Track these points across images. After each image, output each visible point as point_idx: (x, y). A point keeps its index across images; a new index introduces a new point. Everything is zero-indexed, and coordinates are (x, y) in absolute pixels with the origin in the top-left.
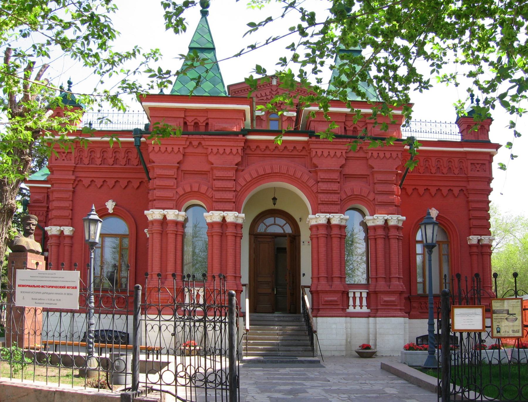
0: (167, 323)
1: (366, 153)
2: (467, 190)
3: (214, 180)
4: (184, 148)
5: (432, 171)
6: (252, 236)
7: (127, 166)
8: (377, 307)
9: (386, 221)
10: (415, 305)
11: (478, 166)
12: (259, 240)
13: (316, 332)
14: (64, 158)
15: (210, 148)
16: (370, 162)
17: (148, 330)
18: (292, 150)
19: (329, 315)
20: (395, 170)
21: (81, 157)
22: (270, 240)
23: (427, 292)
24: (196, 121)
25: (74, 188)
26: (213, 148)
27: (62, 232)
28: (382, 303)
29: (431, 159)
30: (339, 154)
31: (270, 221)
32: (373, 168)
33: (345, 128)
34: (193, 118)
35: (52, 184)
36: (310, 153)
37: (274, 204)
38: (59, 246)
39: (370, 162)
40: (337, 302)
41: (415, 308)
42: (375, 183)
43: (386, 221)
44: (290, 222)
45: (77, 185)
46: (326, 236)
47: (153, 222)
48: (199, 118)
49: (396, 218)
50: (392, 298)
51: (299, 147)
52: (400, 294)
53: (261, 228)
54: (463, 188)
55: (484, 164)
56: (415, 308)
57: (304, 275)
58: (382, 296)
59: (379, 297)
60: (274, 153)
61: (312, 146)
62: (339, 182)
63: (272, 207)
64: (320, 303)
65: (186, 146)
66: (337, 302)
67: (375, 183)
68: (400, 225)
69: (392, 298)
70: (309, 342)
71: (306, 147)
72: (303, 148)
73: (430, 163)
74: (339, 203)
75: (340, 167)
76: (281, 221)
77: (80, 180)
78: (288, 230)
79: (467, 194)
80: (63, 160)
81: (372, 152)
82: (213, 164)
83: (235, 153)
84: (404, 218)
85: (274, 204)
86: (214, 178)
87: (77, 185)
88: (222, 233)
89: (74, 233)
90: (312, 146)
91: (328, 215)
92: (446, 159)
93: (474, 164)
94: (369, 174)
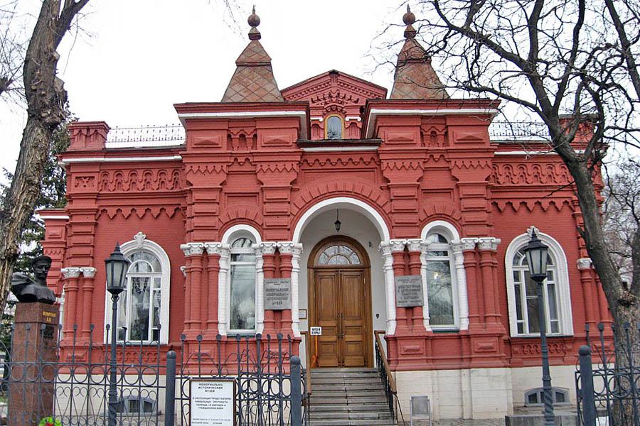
0: (97, 387)
1: (448, 162)
2: (572, 201)
3: (265, 203)
4: (424, 162)
5: (542, 180)
6: (312, 270)
7: (175, 190)
8: (398, 357)
9: (477, 245)
10: (516, 349)
11: (85, 180)
12: (320, 274)
13: (395, 393)
14: (85, 184)
15: (259, 165)
16: (260, 176)
17: (92, 396)
18: (439, 159)
19: (534, 364)
20: (289, 185)
21: (106, 181)
22: (334, 274)
23: (110, 342)
24: (242, 132)
25: (96, 220)
26: (262, 164)
27: (81, 274)
28: (476, 351)
29: (554, 166)
30: (415, 164)
31: (331, 250)
32: (458, 180)
33: (421, 133)
34: (238, 130)
35: (71, 216)
36: (380, 165)
37: (338, 229)
38: (77, 291)
39: (260, 176)
40: (492, 348)
41: (517, 353)
42: (461, 199)
43: (477, 245)
44: (357, 251)
45: (100, 215)
46: (200, 270)
47: (191, 258)
48: (246, 130)
49: (488, 241)
50: (79, 354)
51: (367, 159)
52: (426, 339)
53: (322, 260)
54: (568, 200)
55: (93, 177)
56: (517, 353)
57: (378, 315)
58: (402, 343)
59: (472, 342)
60: (347, 167)
61: (381, 157)
62: (218, 203)
63: (335, 233)
64: (399, 353)
65: (230, 164)
66: (492, 348)
67: (461, 199)
68: (494, 248)
69: (79, 354)
70: (387, 406)
71: (375, 158)
72: (372, 158)
73: (511, 171)
74: (418, 224)
75: (418, 181)
76: (345, 250)
77: (104, 210)
78: (355, 260)
79: (572, 207)
80: (85, 186)
81: (455, 160)
82: (192, 185)
83: (218, 170)
84: (499, 240)
85: (338, 229)
86: (265, 201)
87: (100, 215)
88: (202, 269)
89: (95, 275)
90: (381, 157)
91: (405, 241)
92: (503, 164)
93: (81, 177)
94: (258, 191)
